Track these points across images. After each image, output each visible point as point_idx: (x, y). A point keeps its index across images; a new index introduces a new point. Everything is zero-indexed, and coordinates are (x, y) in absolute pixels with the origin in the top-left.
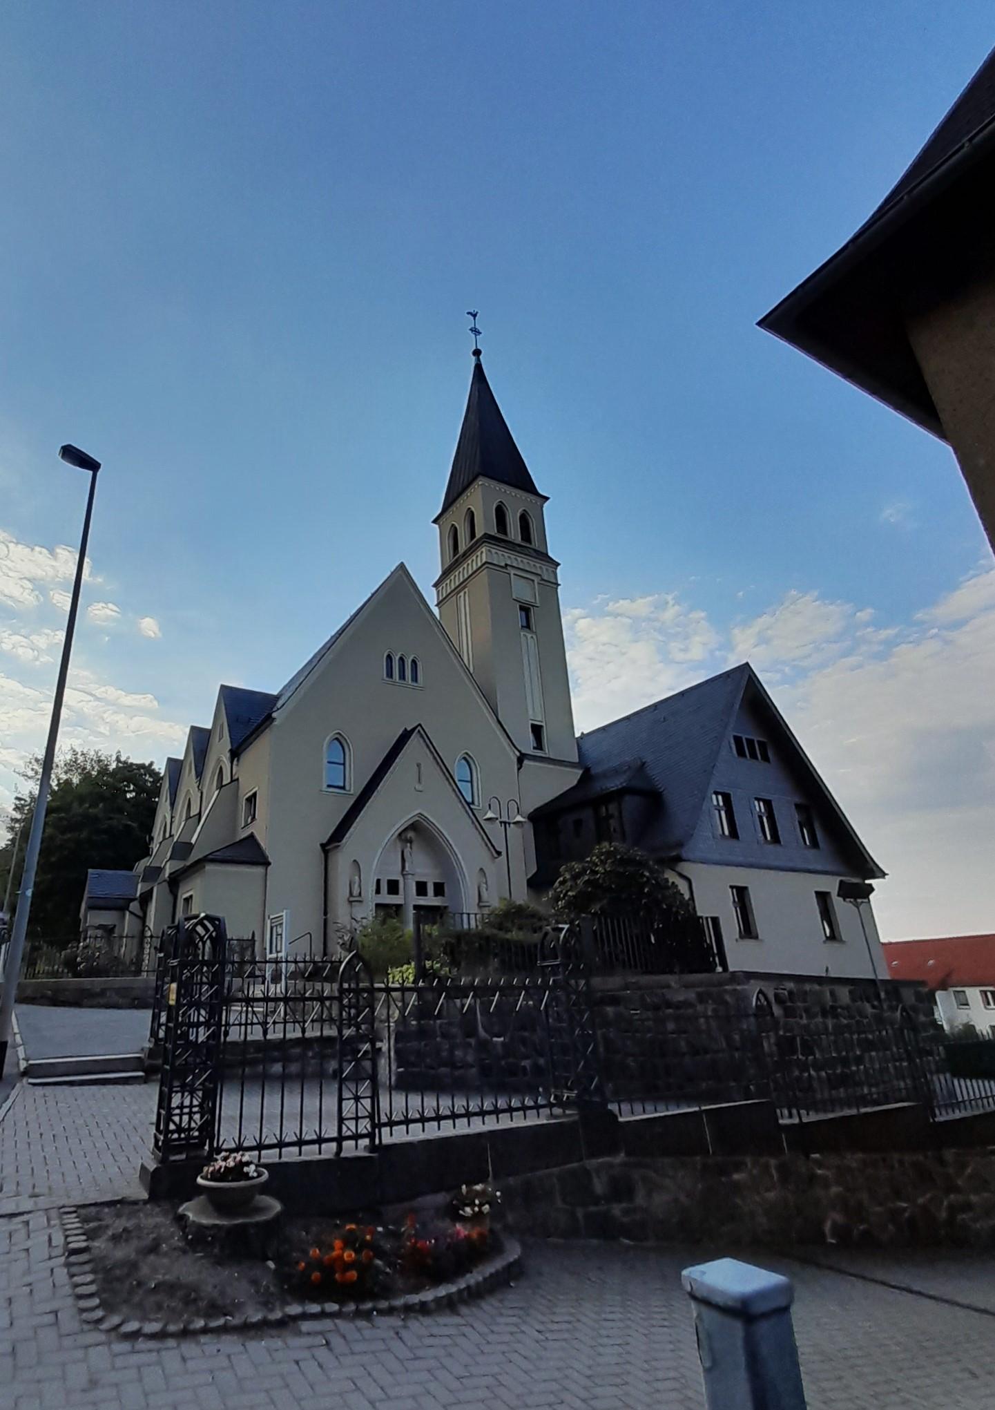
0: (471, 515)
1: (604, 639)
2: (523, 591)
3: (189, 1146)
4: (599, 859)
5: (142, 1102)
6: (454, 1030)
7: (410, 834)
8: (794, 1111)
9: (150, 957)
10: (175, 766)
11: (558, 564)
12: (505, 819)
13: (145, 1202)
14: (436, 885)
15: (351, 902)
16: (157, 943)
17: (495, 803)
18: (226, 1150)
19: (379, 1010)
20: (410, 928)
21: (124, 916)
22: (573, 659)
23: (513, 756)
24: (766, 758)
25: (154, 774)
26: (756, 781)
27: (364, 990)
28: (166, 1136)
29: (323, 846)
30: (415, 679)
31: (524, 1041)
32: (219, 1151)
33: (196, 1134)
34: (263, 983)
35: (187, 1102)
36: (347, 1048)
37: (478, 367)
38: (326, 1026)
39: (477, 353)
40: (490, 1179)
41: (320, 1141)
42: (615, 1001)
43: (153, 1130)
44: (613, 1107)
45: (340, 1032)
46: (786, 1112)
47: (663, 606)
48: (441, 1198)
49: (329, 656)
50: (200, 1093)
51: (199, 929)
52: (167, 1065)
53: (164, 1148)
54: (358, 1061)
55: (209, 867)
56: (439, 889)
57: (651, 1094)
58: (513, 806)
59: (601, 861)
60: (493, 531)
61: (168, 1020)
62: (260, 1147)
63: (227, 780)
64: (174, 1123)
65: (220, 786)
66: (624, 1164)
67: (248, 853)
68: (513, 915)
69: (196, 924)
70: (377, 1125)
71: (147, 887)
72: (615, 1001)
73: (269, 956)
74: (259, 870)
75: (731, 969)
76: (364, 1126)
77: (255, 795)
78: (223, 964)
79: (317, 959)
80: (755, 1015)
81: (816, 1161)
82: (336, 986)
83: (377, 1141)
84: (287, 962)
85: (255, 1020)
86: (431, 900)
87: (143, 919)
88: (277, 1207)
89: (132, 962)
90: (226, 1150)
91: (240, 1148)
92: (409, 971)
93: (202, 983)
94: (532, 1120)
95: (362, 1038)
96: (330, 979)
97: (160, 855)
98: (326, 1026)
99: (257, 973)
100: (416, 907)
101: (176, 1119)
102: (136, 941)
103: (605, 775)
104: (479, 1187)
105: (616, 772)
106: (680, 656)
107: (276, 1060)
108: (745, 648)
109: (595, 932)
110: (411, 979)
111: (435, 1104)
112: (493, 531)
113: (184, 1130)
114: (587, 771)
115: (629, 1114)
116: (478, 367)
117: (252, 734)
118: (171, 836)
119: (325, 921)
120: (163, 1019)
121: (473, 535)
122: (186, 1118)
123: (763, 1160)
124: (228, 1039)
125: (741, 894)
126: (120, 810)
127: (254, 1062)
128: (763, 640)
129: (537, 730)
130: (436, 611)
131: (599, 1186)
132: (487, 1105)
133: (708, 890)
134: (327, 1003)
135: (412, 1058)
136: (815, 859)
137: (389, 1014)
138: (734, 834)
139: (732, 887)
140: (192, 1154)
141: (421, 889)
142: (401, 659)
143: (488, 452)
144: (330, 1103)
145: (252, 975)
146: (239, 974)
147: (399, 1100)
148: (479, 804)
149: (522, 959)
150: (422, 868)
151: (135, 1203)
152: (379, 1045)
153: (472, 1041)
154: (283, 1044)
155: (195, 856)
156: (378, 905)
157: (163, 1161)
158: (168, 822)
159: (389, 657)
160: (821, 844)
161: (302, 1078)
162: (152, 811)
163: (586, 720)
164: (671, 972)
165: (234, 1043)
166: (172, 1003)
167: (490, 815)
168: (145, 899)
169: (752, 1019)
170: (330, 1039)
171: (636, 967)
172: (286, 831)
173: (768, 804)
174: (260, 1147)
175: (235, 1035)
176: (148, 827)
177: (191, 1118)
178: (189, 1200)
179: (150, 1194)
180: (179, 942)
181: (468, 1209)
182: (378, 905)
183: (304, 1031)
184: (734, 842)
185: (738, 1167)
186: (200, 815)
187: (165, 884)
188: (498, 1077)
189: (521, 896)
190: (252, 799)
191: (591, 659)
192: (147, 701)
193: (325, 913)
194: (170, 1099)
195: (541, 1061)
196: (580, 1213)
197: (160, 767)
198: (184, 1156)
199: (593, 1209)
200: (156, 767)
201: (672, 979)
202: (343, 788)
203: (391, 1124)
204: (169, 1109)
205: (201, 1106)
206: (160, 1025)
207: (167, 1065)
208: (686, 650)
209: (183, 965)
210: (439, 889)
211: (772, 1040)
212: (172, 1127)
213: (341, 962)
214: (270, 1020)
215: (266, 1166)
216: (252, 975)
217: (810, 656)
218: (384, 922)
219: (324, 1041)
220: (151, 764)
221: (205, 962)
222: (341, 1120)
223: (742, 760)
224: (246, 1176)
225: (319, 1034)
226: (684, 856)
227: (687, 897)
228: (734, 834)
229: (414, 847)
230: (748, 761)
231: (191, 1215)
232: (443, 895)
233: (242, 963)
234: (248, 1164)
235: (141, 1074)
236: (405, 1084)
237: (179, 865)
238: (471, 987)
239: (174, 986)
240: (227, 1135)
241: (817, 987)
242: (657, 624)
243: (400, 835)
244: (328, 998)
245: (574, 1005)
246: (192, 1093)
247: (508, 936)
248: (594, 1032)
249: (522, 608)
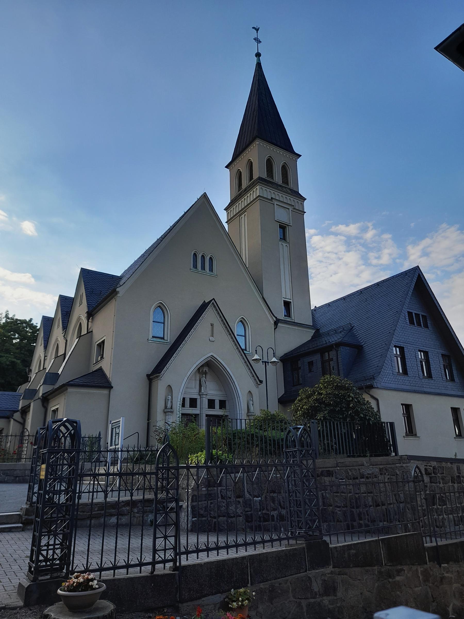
0: (250, 164)
1: (328, 249)
2: (282, 215)
3: (52, 570)
4: (322, 386)
5: (19, 546)
6: (229, 494)
7: (206, 369)
8: (433, 539)
9: (27, 450)
10: (48, 322)
11: (305, 199)
12: (265, 359)
13: (21, 608)
14: (220, 401)
15: (165, 412)
16: (32, 439)
17: (259, 350)
18: (78, 572)
19: (182, 482)
20: (203, 429)
21: (10, 421)
22: (311, 262)
23: (272, 321)
24: (426, 326)
25: (33, 327)
26: (420, 339)
27: (173, 468)
28: (37, 564)
29: (148, 376)
30: (211, 269)
31: (273, 500)
32: (73, 572)
33: (58, 562)
34: (105, 465)
35: (52, 542)
36: (159, 506)
37: (259, 65)
38: (147, 493)
39: (258, 55)
40: (249, 585)
41: (141, 564)
42: (330, 474)
43: (28, 560)
44: (326, 539)
45: (156, 495)
46: (428, 539)
47: (364, 230)
48: (218, 598)
49: (156, 253)
50: (61, 536)
51: (62, 428)
52: (35, 520)
53: (35, 571)
54: (167, 514)
55: (70, 390)
56: (223, 404)
57: (350, 530)
58: (271, 352)
59: (325, 387)
60: (265, 176)
61: (39, 489)
62: (101, 569)
63: (84, 331)
64: (43, 555)
65: (80, 336)
66: (332, 573)
67: (98, 380)
68: (268, 420)
69: (60, 426)
70: (178, 554)
71: (26, 402)
72: (330, 474)
73: (110, 448)
74: (105, 392)
75: (400, 453)
76: (170, 554)
77: (103, 342)
78: (78, 452)
79: (142, 449)
80: (414, 481)
81: (444, 568)
82: (153, 467)
83: (178, 564)
84: (122, 451)
85: (100, 489)
86: (217, 411)
87: (23, 424)
88: (111, 606)
89: (15, 453)
90: (78, 572)
91: (87, 570)
92: (202, 457)
93: (63, 465)
94: (277, 548)
95: (170, 500)
96: (150, 462)
97: (36, 381)
98: (147, 493)
99: (102, 459)
100: (207, 415)
101: (44, 553)
102: (18, 438)
103: (328, 334)
104: (242, 590)
105: (336, 331)
106: (374, 262)
107: (112, 515)
108: (414, 258)
109: (319, 431)
110: (203, 461)
111: (216, 540)
112: (265, 176)
113: (48, 560)
114: (317, 331)
115: (336, 542)
116: (259, 65)
117: (102, 302)
118: (44, 369)
119: (148, 424)
120: (36, 490)
121: (251, 178)
122: (51, 552)
123: (414, 568)
124: (81, 501)
125: (408, 408)
126: (8, 351)
127: (97, 517)
128: (425, 254)
129: (287, 305)
130: (226, 226)
131: (316, 587)
132: (249, 540)
133: (388, 406)
134: (148, 476)
135: (202, 512)
136: (451, 387)
137: (188, 484)
138: (405, 372)
139: (402, 404)
140: (55, 575)
141: (211, 404)
142: (203, 257)
143: (263, 122)
144: (148, 542)
145: (98, 460)
146: (90, 460)
147: (193, 539)
148: (250, 349)
149: (274, 448)
150: (212, 390)
151: (14, 608)
152: (181, 503)
153: (241, 500)
154: (116, 505)
155: (60, 382)
156: (183, 414)
157: (34, 580)
158: (42, 360)
159: (195, 255)
160: (456, 379)
161: (130, 526)
162: (31, 352)
163: (318, 299)
164: (365, 456)
165: (86, 505)
166: (42, 477)
167: (256, 357)
168: (25, 411)
169: (411, 484)
170: (149, 501)
171: (343, 453)
172: (123, 365)
173: (426, 353)
174: (101, 569)
175: (85, 499)
176: (27, 363)
177: (54, 552)
178: (52, 604)
179: (25, 603)
180: (48, 439)
181: (235, 604)
182: (183, 414)
183: (132, 495)
184: (406, 378)
185: (399, 572)
186: (65, 355)
187: (39, 400)
188: (257, 523)
189: (274, 408)
190: (101, 345)
191: (321, 262)
192: (27, 278)
193: (149, 419)
194: (40, 542)
195: (284, 512)
196: (304, 603)
197: (37, 322)
198: (48, 577)
199: (312, 600)
200: (34, 322)
201: (364, 460)
202: (163, 338)
203: (187, 552)
204: (39, 546)
205: (61, 544)
206: (34, 493)
207: (35, 520)
208: (379, 258)
209: (50, 453)
210: (223, 404)
211: (423, 497)
212: (41, 558)
213: (157, 451)
214: (109, 489)
215: (104, 581)
216: (98, 460)
217: (452, 265)
218: (186, 425)
219: (145, 502)
220: (31, 320)
221: (67, 450)
222: (155, 551)
223: (412, 326)
224: (92, 588)
225: (141, 497)
226: (375, 385)
227: (376, 410)
228: (405, 372)
229: (208, 376)
230: (415, 328)
231: (53, 615)
232: (225, 407)
233: (92, 452)
234: (92, 580)
235: (21, 525)
236: (197, 528)
237: (49, 388)
238: (242, 466)
239: (44, 466)
240: (79, 562)
241: (449, 465)
242: (362, 241)
243: (199, 369)
244: (148, 473)
245: (305, 476)
246: (55, 536)
247: (266, 434)
248: (317, 494)
249: (281, 227)
